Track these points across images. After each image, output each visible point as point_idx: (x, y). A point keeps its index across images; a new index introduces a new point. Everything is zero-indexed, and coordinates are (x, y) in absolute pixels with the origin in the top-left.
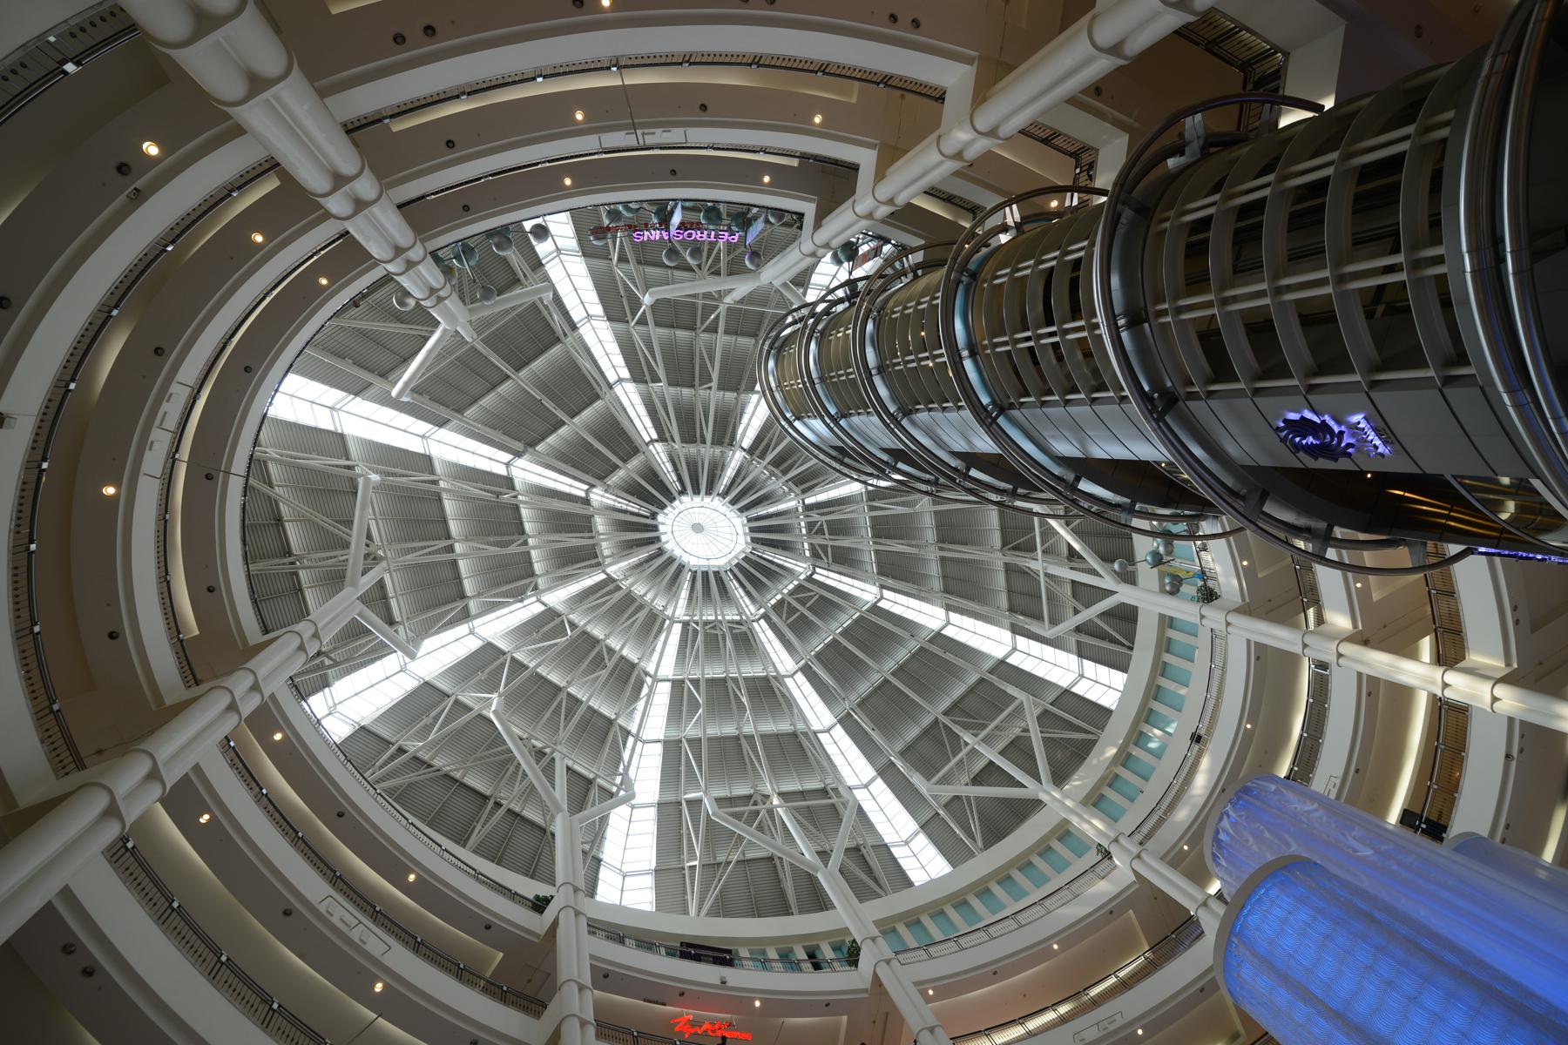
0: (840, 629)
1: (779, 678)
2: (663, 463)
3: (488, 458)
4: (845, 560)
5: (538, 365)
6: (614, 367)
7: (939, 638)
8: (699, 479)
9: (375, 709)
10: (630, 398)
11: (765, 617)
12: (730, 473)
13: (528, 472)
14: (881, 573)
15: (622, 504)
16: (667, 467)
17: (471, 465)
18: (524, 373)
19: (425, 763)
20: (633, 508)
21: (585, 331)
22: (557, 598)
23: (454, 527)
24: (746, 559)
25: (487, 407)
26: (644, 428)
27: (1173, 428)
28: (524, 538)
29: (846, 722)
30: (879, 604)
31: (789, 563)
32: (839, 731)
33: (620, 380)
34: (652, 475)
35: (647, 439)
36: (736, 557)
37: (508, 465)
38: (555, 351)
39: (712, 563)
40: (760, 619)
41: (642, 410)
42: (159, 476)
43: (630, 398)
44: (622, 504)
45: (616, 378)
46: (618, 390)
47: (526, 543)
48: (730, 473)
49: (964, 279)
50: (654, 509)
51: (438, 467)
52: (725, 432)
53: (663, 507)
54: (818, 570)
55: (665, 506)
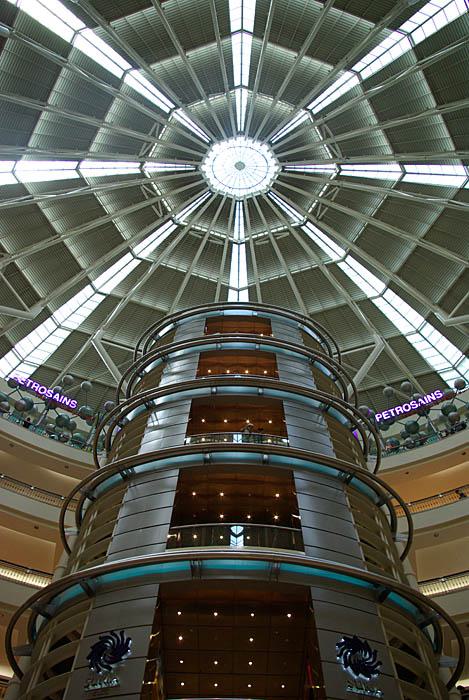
0: (322, 193)
3: (59, 170)
4: (358, 150)
5: (406, 253)
8: (259, 208)
10: (333, 251)
11: (166, 116)
13: (93, 169)
14: (396, 150)
15: (171, 167)
16: (285, 207)
17: (443, 166)
18: (413, 245)
20: (180, 168)
21: (381, 286)
22: (302, 117)
23: (57, 226)
24: (259, 198)
29: (65, 48)
31: (319, 169)
32: (67, 36)
33: (343, 260)
34: (296, 200)
37: (405, 173)
38: (397, 266)
39: (253, 190)
40: (170, 113)
43: (333, 251)
44: (171, 167)
45: (347, 260)
46: (342, 253)
51: (30, 189)
52: (261, 255)
53: (200, 159)
54: (343, 167)
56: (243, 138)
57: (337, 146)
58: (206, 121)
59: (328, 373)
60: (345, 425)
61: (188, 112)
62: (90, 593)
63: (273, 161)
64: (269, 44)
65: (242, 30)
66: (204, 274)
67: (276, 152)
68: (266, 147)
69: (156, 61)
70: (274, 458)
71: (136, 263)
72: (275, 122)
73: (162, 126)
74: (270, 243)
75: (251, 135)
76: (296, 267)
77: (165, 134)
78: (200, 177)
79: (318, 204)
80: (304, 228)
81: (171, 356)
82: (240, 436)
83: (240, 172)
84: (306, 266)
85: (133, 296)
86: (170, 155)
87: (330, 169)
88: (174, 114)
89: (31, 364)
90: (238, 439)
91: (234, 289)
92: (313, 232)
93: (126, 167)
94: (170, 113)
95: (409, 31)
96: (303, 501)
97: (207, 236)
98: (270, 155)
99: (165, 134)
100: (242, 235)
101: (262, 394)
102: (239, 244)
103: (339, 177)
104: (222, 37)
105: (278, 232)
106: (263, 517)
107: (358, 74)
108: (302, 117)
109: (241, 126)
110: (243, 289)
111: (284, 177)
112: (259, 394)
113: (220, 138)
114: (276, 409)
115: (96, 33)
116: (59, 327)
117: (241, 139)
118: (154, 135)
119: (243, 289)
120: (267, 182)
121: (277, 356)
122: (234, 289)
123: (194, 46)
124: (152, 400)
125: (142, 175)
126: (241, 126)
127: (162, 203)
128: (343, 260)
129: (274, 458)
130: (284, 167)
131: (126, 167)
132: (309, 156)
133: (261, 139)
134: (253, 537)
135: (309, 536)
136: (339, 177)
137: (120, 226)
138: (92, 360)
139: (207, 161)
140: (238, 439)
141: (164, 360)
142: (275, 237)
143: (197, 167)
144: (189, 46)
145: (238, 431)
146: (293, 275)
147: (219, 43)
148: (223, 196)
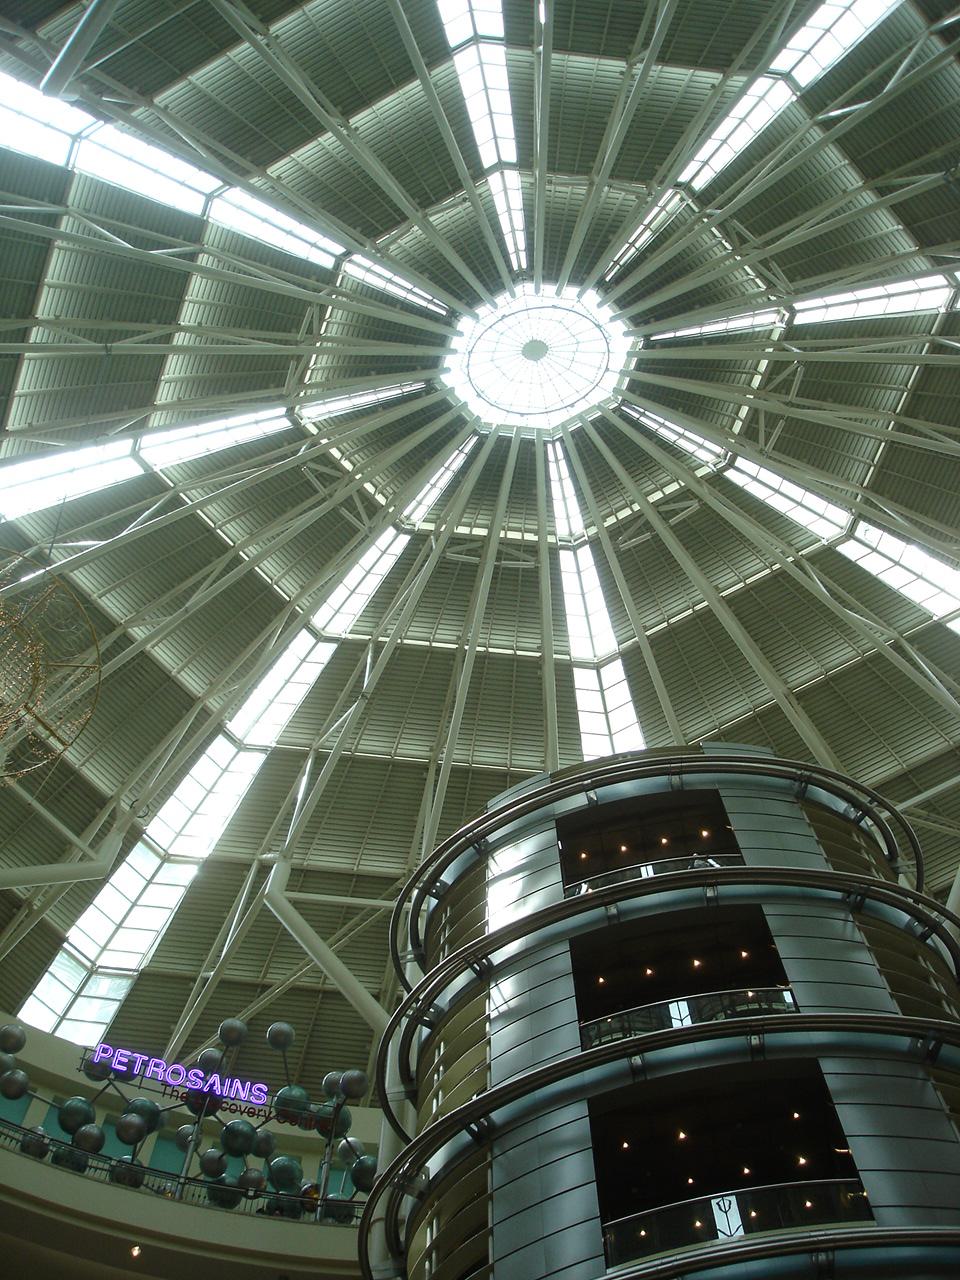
1: (140, 427)
2: (681, 436)
6: (897, 563)
7: (829, 560)
9: (142, 446)
11: (328, 277)
12: (440, 479)
19: (257, 985)
24: (602, 425)
25: (245, 68)
26: (755, 478)
27: (777, 779)
28: (259, 26)
30: (841, 549)
33: (850, 534)
35: (740, 462)
36: (580, 417)
40: (337, 266)
41: (778, 503)
42: (314, 641)
45: (859, 533)
46: (843, 517)
47: (192, 257)
48: (440, 479)
49: (853, 897)
50: (426, 374)
53: (433, 363)
55: (638, 368)
56: (529, 286)
57: (773, 265)
58: (429, 267)
59: (841, 806)
60: (909, 928)
61: (382, 257)
62: (486, 1138)
63: (621, 326)
64: (554, 56)
65: (476, 39)
66: (501, 644)
67: (623, 303)
68: (592, 296)
69: (279, 156)
70: (772, 1039)
71: (326, 651)
72: (608, 230)
73: (323, 308)
74: (656, 538)
75: (552, 273)
76: (730, 577)
77: (334, 322)
78: (443, 406)
79: (754, 413)
80: (730, 474)
81: (491, 838)
82: (650, 868)
83: (544, 360)
84: (757, 572)
85: (333, 740)
86: (356, 370)
87: (768, 320)
88: (347, 267)
89: (119, 973)
90: (647, 872)
91: (584, 665)
92: (755, 478)
93: (259, 423)
94: (337, 266)
95: (602, 670)
96: (850, 1118)
97: (493, 549)
98: (607, 311)
99: (334, 322)
100: (578, 526)
101: (716, 899)
102: (574, 549)
103: (717, 480)
104: (431, 65)
105: (667, 500)
106: (773, 1167)
107: (787, 77)
108: (669, 204)
109: (519, 260)
110: (610, 660)
111: (654, 361)
112: (709, 899)
113: (471, 300)
114: (749, 925)
115: (116, 127)
116: (166, 858)
117: (525, 289)
118: (310, 331)
119: (610, 660)
120: (612, 381)
121: (722, 793)
122: (584, 665)
123: (364, 101)
124: (431, 1004)
125: (419, 539)
126: (519, 260)
127: (362, 493)
128: (850, 534)
129: (772, 1039)
130: (647, 337)
131: (259, 423)
132: (713, 297)
133: (579, 278)
134: (762, 1215)
135: (876, 1188)
136: (717, 480)
137: (269, 570)
138: (267, 936)
139: (449, 361)
140: (647, 872)
141: (478, 851)
142: (666, 516)
143: (428, 382)
144: (353, 101)
145: (646, 860)
146: (730, 601)
147: (425, 82)
148: (509, 440)
